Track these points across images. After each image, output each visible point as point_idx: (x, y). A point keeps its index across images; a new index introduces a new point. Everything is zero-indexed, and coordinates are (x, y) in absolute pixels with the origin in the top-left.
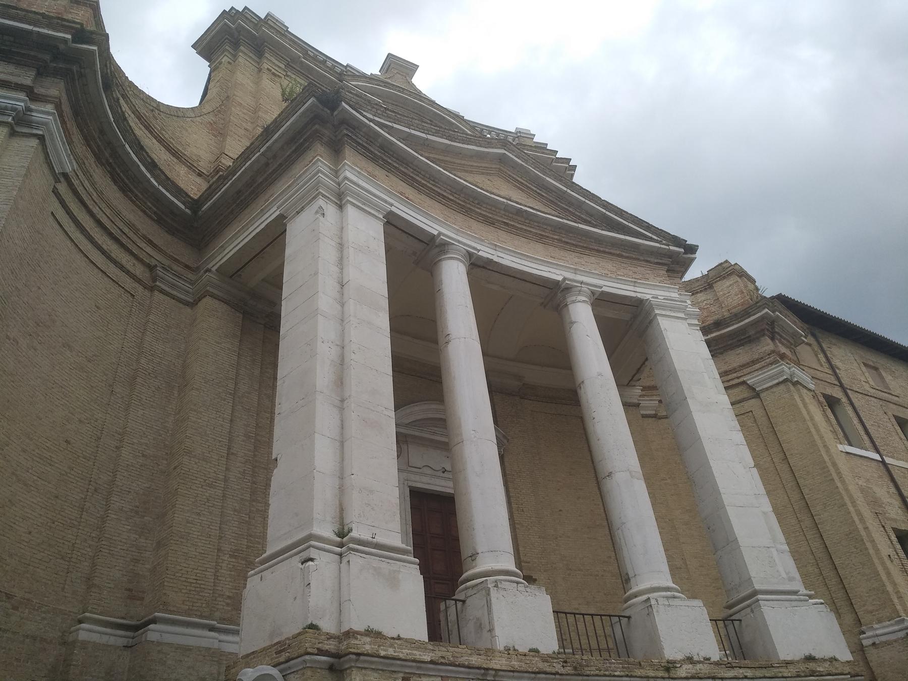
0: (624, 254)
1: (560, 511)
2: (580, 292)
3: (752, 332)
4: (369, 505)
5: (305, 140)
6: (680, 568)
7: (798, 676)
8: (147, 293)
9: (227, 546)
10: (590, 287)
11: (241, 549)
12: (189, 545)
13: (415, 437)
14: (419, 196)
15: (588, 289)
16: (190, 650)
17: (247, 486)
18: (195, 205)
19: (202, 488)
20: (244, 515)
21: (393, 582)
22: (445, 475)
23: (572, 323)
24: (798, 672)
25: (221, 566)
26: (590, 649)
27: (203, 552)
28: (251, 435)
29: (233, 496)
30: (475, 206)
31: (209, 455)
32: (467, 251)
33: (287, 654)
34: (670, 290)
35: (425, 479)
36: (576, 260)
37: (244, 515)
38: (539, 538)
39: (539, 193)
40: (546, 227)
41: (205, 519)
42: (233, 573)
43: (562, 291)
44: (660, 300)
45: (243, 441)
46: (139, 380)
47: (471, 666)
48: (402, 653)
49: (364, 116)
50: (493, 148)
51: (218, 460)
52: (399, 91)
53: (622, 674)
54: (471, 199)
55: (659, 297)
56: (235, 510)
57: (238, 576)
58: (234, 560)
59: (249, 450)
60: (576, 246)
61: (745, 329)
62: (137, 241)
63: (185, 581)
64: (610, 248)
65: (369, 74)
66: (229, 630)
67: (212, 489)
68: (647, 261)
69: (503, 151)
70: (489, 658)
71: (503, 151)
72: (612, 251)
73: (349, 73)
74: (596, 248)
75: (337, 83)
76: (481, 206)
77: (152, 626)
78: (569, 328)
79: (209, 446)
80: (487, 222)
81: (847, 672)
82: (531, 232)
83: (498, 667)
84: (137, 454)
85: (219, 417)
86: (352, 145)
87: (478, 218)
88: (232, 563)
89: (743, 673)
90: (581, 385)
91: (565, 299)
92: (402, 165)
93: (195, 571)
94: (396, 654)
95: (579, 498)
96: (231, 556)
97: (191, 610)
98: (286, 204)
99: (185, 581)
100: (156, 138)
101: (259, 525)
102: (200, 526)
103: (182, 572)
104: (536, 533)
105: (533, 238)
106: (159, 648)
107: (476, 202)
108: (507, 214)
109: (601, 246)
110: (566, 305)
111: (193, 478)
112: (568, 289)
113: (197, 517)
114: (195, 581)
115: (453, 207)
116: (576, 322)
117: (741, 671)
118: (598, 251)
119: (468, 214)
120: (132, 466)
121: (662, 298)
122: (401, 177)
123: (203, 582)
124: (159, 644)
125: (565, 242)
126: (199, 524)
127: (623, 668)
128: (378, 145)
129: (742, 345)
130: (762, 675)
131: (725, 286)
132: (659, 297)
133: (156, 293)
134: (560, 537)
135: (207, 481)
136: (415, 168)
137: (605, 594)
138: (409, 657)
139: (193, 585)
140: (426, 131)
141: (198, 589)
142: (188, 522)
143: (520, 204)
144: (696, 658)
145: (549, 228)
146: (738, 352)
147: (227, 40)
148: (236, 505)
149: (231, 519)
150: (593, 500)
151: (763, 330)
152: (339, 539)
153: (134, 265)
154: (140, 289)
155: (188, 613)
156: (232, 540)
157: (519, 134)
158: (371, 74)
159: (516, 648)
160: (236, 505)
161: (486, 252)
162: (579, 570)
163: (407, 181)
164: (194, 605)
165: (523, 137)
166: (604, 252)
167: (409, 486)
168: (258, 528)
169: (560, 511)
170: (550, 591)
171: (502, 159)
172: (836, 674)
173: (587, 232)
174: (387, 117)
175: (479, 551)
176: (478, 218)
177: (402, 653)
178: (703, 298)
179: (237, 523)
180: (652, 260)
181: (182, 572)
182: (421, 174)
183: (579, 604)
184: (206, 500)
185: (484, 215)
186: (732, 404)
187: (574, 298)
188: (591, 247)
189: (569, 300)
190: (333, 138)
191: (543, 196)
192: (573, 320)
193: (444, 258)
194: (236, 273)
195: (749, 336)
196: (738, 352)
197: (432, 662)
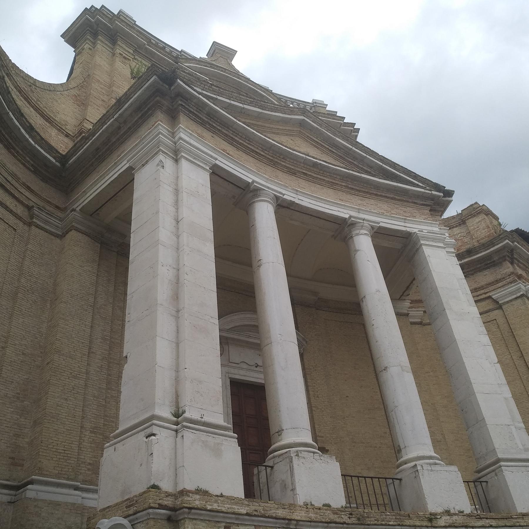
0: (396, 197)
1: (347, 397)
3: (496, 258)
5: (149, 109)
8: (26, 228)
9: (88, 424)
10: (370, 223)
11: (99, 426)
12: (59, 423)
13: (233, 339)
15: (369, 224)
16: (59, 505)
18: (63, 159)
19: (68, 379)
21: (217, 452)
23: (357, 251)
25: (84, 440)
26: (370, 504)
27: (69, 429)
29: (93, 385)
31: (74, 354)
32: (275, 195)
33: (135, 508)
34: (433, 225)
35: (242, 372)
37: (101, 400)
38: (331, 418)
39: (330, 150)
41: (71, 403)
42: (93, 445)
43: (349, 226)
44: (425, 233)
45: (101, 342)
46: (20, 295)
48: (224, 507)
49: (195, 90)
50: (295, 115)
51: (82, 357)
53: (395, 523)
54: (278, 155)
56: (94, 397)
58: (93, 435)
59: (105, 350)
60: (359, 191)
61: (490, 256)
63: (56, 451)
64: (385, 192)
66: (90, 490)
67: (76, 380)
68: (415, 203)
69: (302, 117)
70: (292, 511)
71: (302, 117)
72: (388, 195)
74: (375, 193)
75: (174, 65)
76: (286, 160)
77: (30, 486)
78: (353, 255)
79: (74, 346)
80: (290, 172)
82: (324, 180)
83: (299, 518)
84: (19, 353)
85: (82, 324)
89: (489, 523)
90: (364, 300)
91: (350, 232)
93: (63, 443)
94: (219, 508)
95: (362, 386)
96: (91, 432)
97: (60, 474)
99: (56, 451)
101: (113, 408)
102: (68, 408)
103: (53, 444)
105: (326, 184)
106: (36, 504)
107: (282, 157)
109: (378, 191)
110: (352, 237)
111: (61, 371)
113: (65, 402)
114: (63, 451)
116: (359, 250)
117: (487, 521)
118: (376, 195)
119: (275, 166)
120: (14, 362)
123: (69, 452)
124: (35, 500)
126: (66, 407)
127: (396, 518)
128: (206, 113)
129: (488, 268)
131: (475, 222)
132: (424, 231)
133: (33, 227)
135: (73, 374)
136: (234, 130)
137: (382, 462)
139: (62, 454)
140: (242, 102)
141: (65, 458)
142: (58, 406)
143: (316, 159)
144: (452, 511)
145: (339, 177)
146: (485, 274)
148: (95, 392)
149: (91, 403)
150: (373, 388)
151: (504, 256)
152: (175, 419)
153: (16, 206)
154: (21, 224)
155: (58, 476)
156: (93, 420)
157: (315, 105)
159: (313, 503)
160: (95, 392)
161: (289, 196)
164: (63, 470)
166: (381, 196)
167: (230, 378)
168: (112, 410)
169: (347, 397)
170: (339, 459)
171: (302, 124)
174: (213, 91)
175: (284, 428)
176: (283, 169)
177: (224, 507)
178: (458, 232)
179: (96, 406)
180: (418, 202)
181: (53, 444)
183: (362, 469)
184: (72, 389)
186: (481, 314)
187: (358, 232)
188: (371, 192)
189: (354, 233)
190: (171, 107)
191: (333, 152)
192: (357, 248)
194: (95, 212)
195: (494, 261)
196: (485, 274)
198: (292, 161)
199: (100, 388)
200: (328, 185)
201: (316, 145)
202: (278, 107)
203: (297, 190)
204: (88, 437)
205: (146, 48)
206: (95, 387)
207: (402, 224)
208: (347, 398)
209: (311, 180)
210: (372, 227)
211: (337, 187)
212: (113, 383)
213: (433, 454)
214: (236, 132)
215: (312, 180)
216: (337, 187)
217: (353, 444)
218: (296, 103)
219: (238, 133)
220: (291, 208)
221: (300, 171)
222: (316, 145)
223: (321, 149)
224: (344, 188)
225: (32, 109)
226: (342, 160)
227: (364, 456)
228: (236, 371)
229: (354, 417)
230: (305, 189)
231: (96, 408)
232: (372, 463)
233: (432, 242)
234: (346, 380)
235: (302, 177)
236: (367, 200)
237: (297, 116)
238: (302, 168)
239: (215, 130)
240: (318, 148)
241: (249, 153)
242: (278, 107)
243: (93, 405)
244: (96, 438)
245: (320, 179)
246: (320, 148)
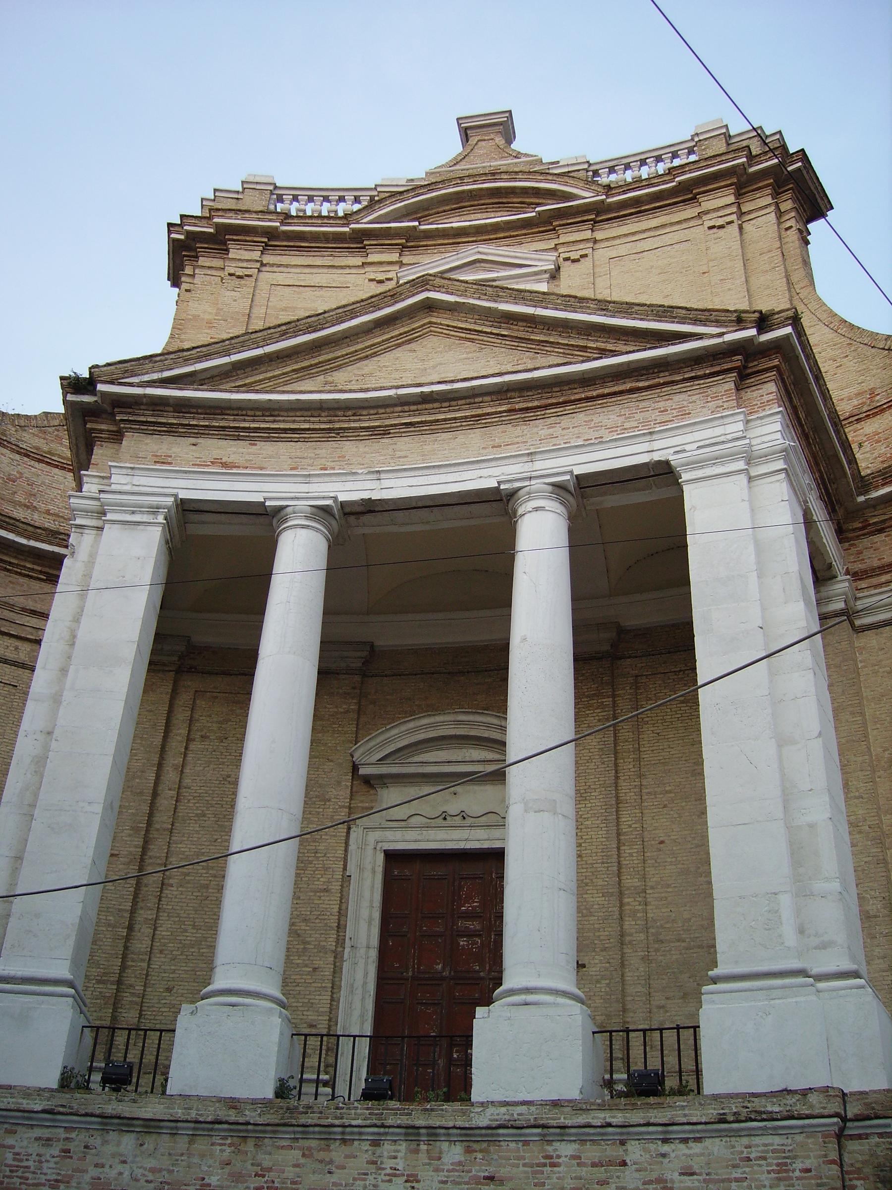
1: (662, 842)
2: (530, 496)
4: (30, 931)
6: (876, 917)
7: (723, 1121)
9: (94, 970)
11: (112, 971)
14: (253, 449)
17: (128, 893)
20: (120, 930)
22: (449, 821)
24: (724, 1114)
28: (141, 825)
30: (350, 421)
34: (726, 421)
35: (412, 835)
36: (545, 432)
37: (120, 930)
38: (603, 896)
39: (498, 335)
40: (480, 399)
44: (692, 450)
45: (130, 835)
47: (106, 1115)
49: (131, 385)
52: (457, 185)
55: (687, 447)
56: (109, 925)
57: (105, 1004)
59: (136, 847)
60: (546, 407)
62: (14, 618)
65: (424, 176)
73: (383, 196)
80: (375, 435)
81: (832, 1112)
82: (455, 419)
86: (134, 429)
87: (359, 436)
88: (99, 990)
92: (214, 419)
96: (99, 982)
98: (246, 425)
100: (57, 466)
101: (146, 938)
104: (597, 890)
105: (462, 426)
108: (406, 408)
112: (512, 494)
115: (313, 438)
118: (588, 399)
119: (341, 437)
121: (695, 446)
122: (218, 435)
125: (521, 410)
130: (642, 1121)
132: (687, 447)
134: (652, 888)
138: (12, 1106)
147: (185, 258)
153: (17, 648)
157: (696, 139)
158: (427, 173)
160: (111, 918)
162: (679, 941)
163: (229, 435)
165: (706, 139)
168: (143, 942)
169: (662, 842)
170: (607, 981)
172: (808, 1117)
173: (556, 377)
176: (359, 436)
179: (111, 940)
182: (248, 416)
183: (667, 999)
185: (368, 427)
193: (281, 531)
197: (44, 1111)
198: (372, 412)
199: (120, 910)
200: (469, 425)
201: (468, 336)
202: (355, 306)
203: (378, 472)
204: (93, 989)
205: (285, 232)
206: (111, 910)
207: (645, 447)
208: (662, 845)
209: (426, 430)
210: (558, 486)
211: (490, 420)
212: (150, 897)
213: (278, 994)
214: (240, 412)
215: (429, 430)
216: (490, 420)
217: (657, 946)
218: (652, 159)
219: (244, 412)
220: (376, 509)
221: (395, 425)
222: (468, 336)
223: (479, 340)
224: (507, 416)
225: (56, 471)
226: (525, 345)
227: (678, 969)
228: (398, 835)
229: (669, 886)
230: (406, 457)
231: (110, 944)
232: (695, 983)
233: (714, 468)
234: (665, 806)
235: (404, 432)
236: (566, 421)
237: (410, 299)
238: (399, 417)
239: (196, 431)
240: (472, 340)
241: (278, 438)
242: (355, 306)
243: (104, 940)
244: (105, 990)
245: (445, 420)
246: (476, 340)
